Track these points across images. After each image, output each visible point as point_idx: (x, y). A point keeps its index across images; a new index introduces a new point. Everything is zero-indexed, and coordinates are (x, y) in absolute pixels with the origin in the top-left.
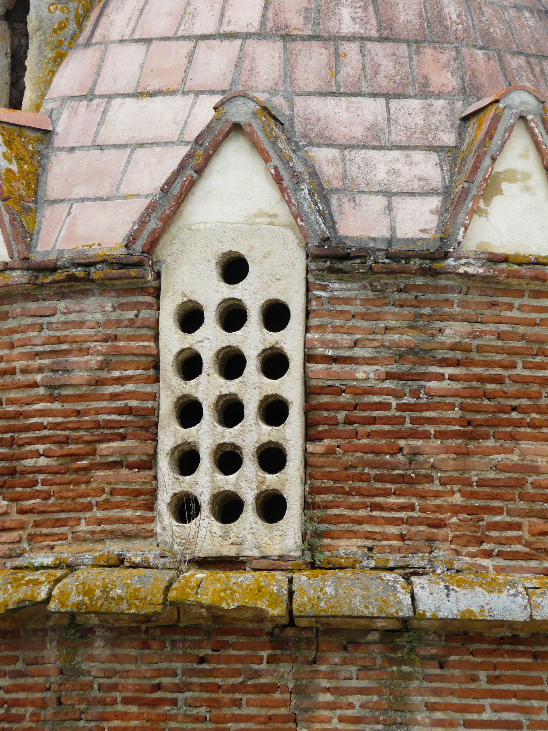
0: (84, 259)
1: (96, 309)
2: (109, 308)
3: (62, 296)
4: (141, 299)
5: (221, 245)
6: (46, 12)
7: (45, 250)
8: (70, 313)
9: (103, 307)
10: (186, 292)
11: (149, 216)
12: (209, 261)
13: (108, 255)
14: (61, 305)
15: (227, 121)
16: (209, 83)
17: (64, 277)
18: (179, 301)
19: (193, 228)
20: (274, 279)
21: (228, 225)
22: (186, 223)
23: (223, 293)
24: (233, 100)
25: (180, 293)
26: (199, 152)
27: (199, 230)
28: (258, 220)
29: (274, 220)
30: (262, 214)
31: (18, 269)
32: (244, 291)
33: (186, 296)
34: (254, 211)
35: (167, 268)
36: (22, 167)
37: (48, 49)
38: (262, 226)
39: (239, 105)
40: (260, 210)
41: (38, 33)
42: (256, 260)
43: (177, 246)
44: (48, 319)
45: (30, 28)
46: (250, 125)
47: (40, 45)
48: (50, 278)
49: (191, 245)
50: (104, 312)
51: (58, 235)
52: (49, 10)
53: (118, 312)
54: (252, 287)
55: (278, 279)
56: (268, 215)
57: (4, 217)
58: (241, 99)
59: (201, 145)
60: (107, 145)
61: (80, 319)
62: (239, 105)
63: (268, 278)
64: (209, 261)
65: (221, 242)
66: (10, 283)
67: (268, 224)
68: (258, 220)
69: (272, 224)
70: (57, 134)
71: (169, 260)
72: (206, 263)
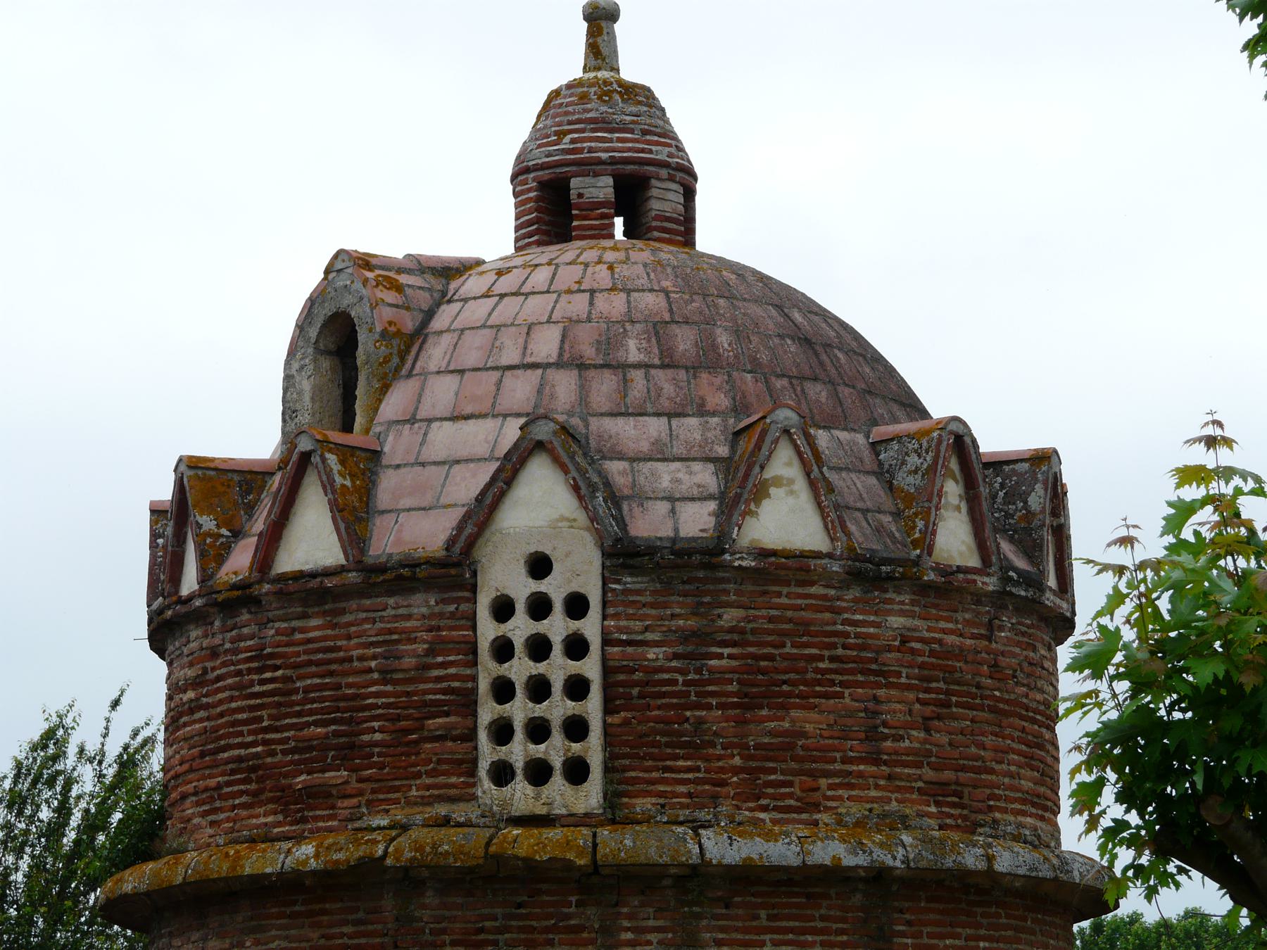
2: (432, 603)
3: (391, 594)
9: (427, 602)
14: (391, 601)
30: (563, 519)
34: (556, 516)
53: (441, 606)
56: (568, 520)
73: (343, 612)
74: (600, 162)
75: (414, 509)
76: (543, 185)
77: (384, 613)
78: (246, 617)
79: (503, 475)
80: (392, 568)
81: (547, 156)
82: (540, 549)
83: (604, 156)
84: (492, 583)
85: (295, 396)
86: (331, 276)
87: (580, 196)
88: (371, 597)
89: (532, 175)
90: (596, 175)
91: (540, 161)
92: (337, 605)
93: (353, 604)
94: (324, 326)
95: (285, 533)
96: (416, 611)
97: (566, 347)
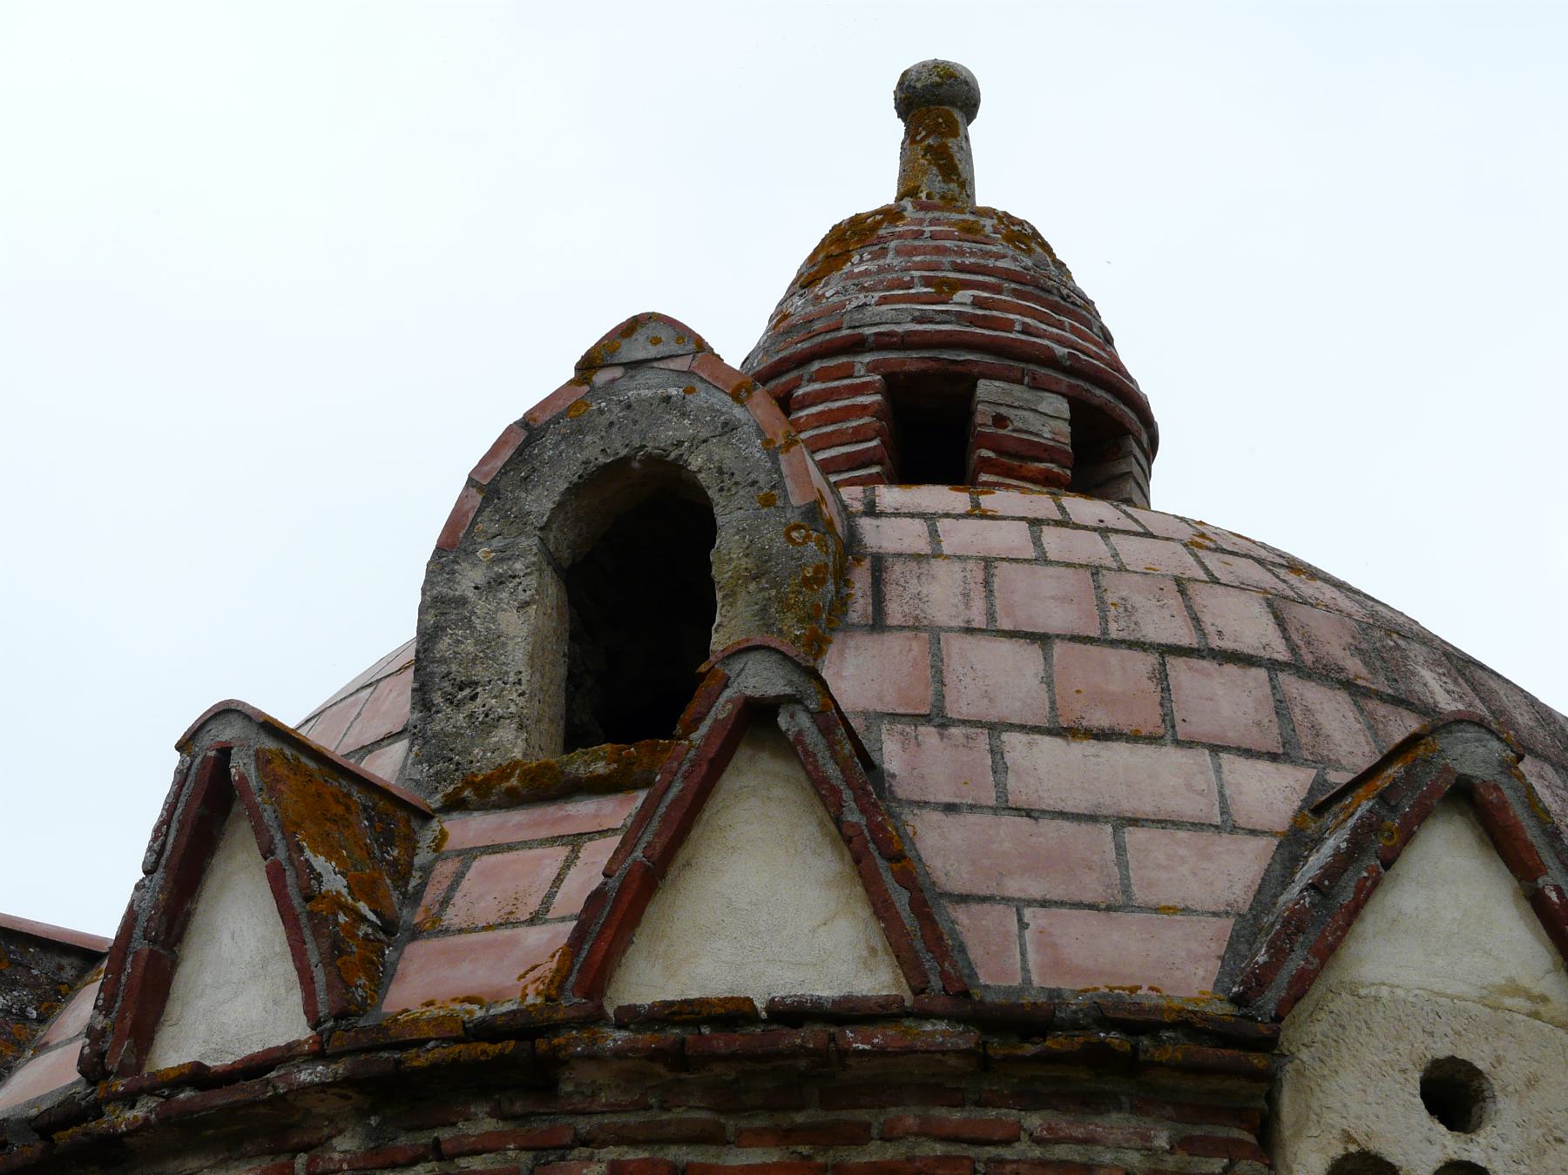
0: (1130, 1012)
1: (1128, 1140)
2: (1162, 1141)
3: (1031, 1100)
4: (1221, 1132)
5: (1429, 1040)
6: (780, 542)
7: (1005, 984)
8: (1058, 1141)
9: (1146, 1138)
10: (1352, 1132)
11: (1292, 943)
12: (1404, 1071)
13: (1195, 1013)
14: (1034, 1121)
15: (1446, 768)
16: (1230, 734)
17: (1077, 1047)
18: (1338, 1151)
19: (1363, 992)
20: (1550, 1138)
21: (1442, 1000)
22: (1347, 979)
23: (1445, 1147)
24: (1454, 728)
25: (1336, 1133)
26: (1388, 822)
27: (1377, 999)
28: (1509, 1002)
29: (1542, 1008)
30: (1515, 989)
31: (941, 1017)
32: (1491, 1152)
33: (1354, 1141)
34: (1499, 980)
35: (1300, 1073)
36: (348, 986)
37: (790, 620)
38: (1516, 1016)
39: (1467, 741)
40: (1512, 980)
41: (752, 587)
42: (1511, 1089)
43: (1324, 1026)
44: (992, 1151)
45: (722, 572)
46: (1497, 788)
47: (764, 609)
48: (1029, 1049)
49: (1359, 1029)
50: (1150, 1151)
51: (1023, 954)
52: (790, 539)
53: (1181, 1157)
54: (1507, 1146)
55: (1560, 1140)
56: (1529, 996)
57: (894, 897)
58: (1472, 729)
59: (1393, 809)
60: (1044, 812)
61: (1085, 1159)
62: (1467, 741)
63: (1539, 1132)
64: (1404, 1071)
65: (1432, 1034)
66: (919, 1045)
67: (1529, 1015)
68: (1509, 1002)
69: (1535, 1015)
70: (893, 776)
71: (1304, 1055)
72: (1398, 1076)
73: (858, 1136)
74: (1051, 361)
75: (1061, 904)
76: (894, 384)
77: (1007, 1153)
78: (484, 1124)
79: (1381, 843)
80: (1073, 1025)
81: (915, 320)
82: (1463, 1054)
83: (1061, 351)
84: (1331, 1118)
85: (469, 646)
86: (601, 377)
87: (1000, 421)
88: (960, 1105)
89: (868, 358)
90: (1037, 386)
91: (899, 329)
92: (844, 1115)
93: (910, 1117)
94: (574, 490)
95: (652, 910)
96: (1108, 1157)
97: (1296, 638)
